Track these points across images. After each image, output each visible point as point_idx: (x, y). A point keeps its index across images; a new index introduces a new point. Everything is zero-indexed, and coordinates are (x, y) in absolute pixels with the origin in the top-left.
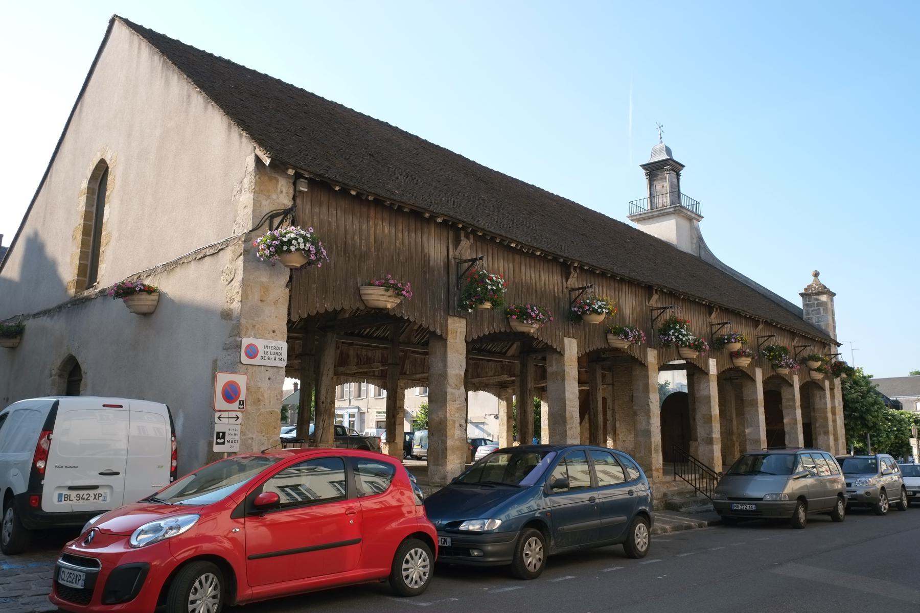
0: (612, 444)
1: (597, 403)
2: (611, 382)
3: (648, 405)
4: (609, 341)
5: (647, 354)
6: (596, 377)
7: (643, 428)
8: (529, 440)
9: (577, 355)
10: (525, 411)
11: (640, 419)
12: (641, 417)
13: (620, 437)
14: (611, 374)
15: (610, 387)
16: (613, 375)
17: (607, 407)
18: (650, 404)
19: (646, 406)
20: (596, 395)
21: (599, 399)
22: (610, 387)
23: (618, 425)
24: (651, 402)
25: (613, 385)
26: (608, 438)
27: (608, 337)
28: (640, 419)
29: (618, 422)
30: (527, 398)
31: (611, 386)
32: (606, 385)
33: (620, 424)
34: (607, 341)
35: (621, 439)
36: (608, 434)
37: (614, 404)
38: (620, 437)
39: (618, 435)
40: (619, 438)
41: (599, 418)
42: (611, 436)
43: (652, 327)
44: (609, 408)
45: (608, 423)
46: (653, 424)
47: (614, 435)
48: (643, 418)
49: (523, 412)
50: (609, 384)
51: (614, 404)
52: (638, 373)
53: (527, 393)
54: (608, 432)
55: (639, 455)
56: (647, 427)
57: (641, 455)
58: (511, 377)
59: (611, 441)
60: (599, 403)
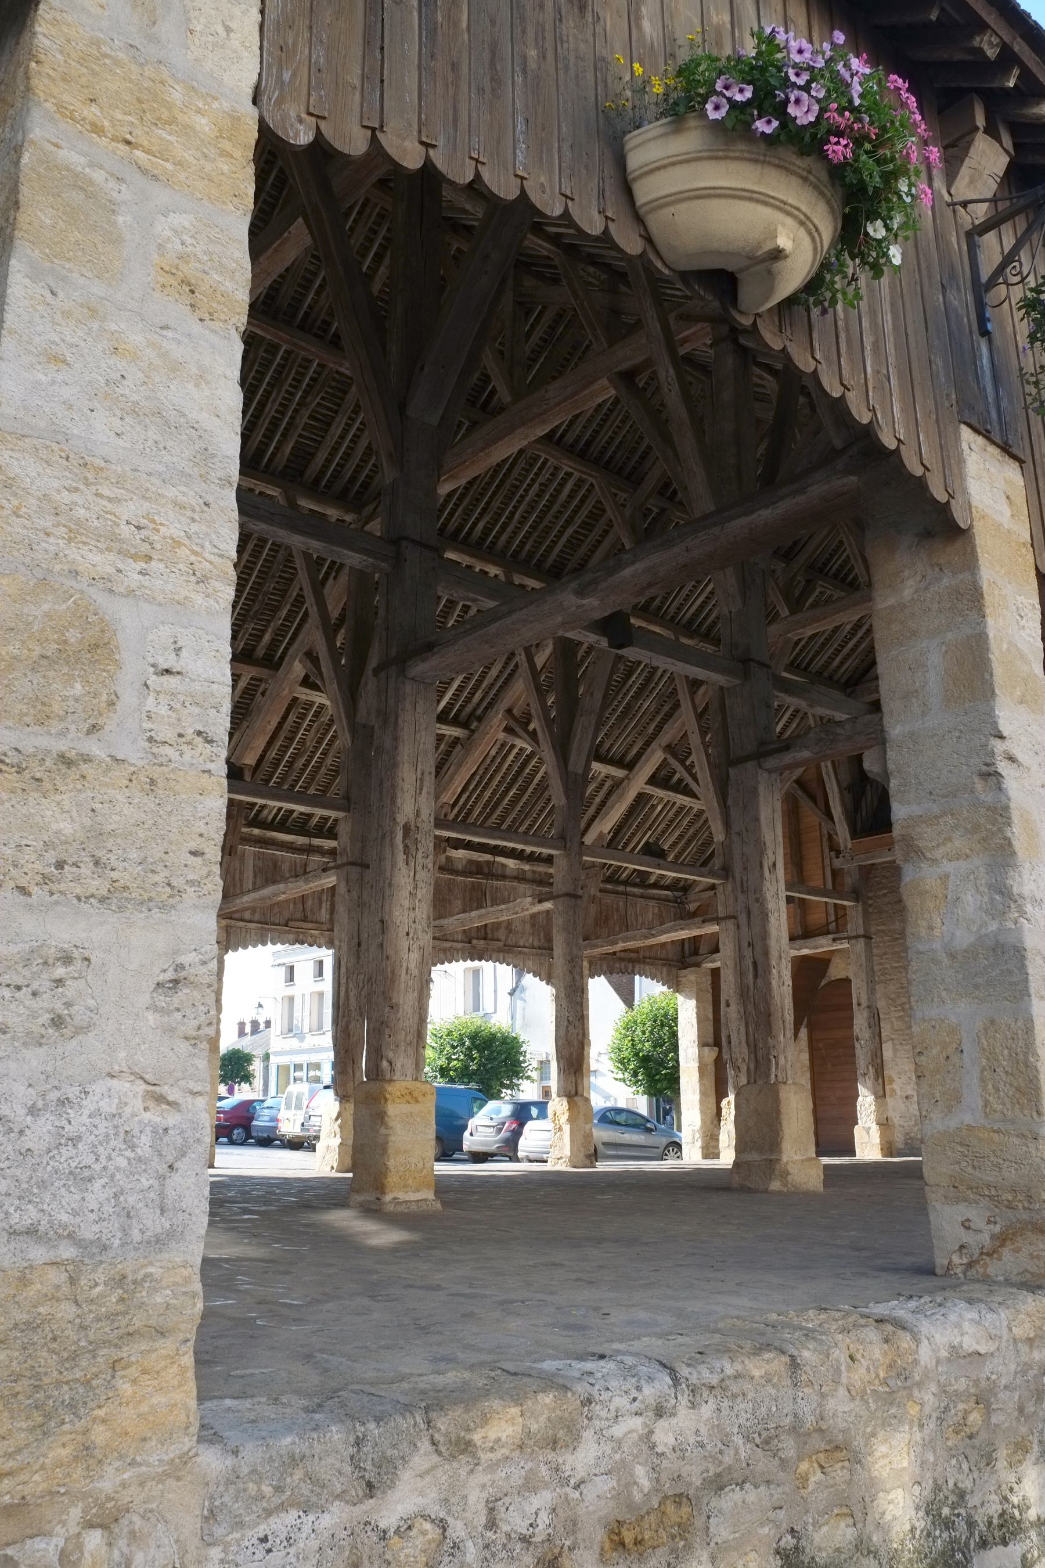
0: (873, 1108)
1: (765, 916)
2: (861, 932)
3: (991, 776)
4: (645, 192)
5: (961, 462)
6: (757, 820)
7: (963, 939)
8: (398, 1065)
9: (250, 115)
10: (382, 921)
11: (945, 878)
12: (947, 867)
13: (895, 1086)
14: (860, 908)
15: (861, 944)
16: (865, 913)
17: (855, 1001)
18: (1003, 767)
19: (979, 785)
20: (759, 890)
21: (771, 905)
22: (861, 944)
23: (888, 1052)
24: (1011, 759)
25: (868, 937)
26: (861, 1089)
27: (635, 161)
28: (945, 878)
29: (890, 1043)
30: (393, 867)
31: (862, 940)
32: (849, 938)
33: (895, 1051)
34: (627, 190)
35: (899, 1093)
36: (860, 1079)
37: (872, 992)
38: (895, 1086)
39: (892, 1081)
40: (893, 1090)
41: (774, 983)
42: (869, 1083)
43: (982, 320)
44: (859, 1005)
45: (857, 1045)
46: (1036, 902)
47: (876, 1080)
48: (963, 865)
49: (378, 926)
50: (857, 937)
51: (872, 992)
52: (907, 593)
53: (392, 839)
54: (860, 1071)
55: (953, 1123)
56: (993, 926)
57: (968, 1119)
58: (540, 902)
59: (871, 1098)
60: (773, 920)
